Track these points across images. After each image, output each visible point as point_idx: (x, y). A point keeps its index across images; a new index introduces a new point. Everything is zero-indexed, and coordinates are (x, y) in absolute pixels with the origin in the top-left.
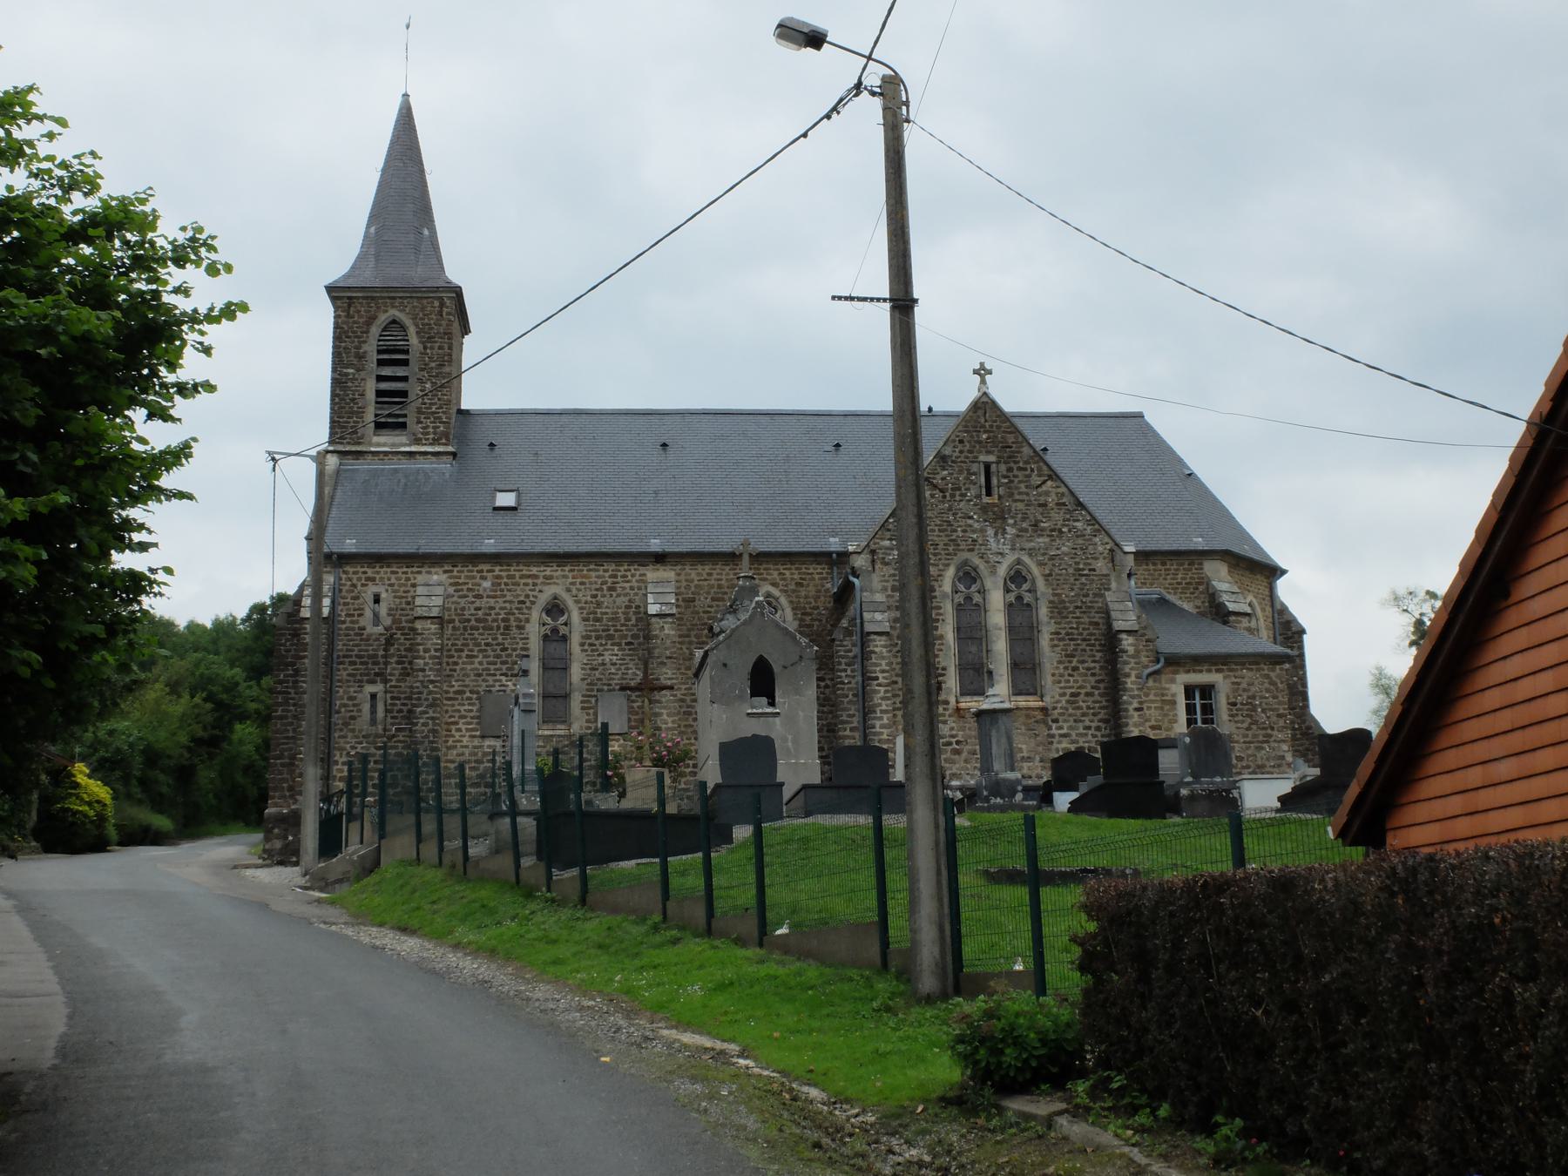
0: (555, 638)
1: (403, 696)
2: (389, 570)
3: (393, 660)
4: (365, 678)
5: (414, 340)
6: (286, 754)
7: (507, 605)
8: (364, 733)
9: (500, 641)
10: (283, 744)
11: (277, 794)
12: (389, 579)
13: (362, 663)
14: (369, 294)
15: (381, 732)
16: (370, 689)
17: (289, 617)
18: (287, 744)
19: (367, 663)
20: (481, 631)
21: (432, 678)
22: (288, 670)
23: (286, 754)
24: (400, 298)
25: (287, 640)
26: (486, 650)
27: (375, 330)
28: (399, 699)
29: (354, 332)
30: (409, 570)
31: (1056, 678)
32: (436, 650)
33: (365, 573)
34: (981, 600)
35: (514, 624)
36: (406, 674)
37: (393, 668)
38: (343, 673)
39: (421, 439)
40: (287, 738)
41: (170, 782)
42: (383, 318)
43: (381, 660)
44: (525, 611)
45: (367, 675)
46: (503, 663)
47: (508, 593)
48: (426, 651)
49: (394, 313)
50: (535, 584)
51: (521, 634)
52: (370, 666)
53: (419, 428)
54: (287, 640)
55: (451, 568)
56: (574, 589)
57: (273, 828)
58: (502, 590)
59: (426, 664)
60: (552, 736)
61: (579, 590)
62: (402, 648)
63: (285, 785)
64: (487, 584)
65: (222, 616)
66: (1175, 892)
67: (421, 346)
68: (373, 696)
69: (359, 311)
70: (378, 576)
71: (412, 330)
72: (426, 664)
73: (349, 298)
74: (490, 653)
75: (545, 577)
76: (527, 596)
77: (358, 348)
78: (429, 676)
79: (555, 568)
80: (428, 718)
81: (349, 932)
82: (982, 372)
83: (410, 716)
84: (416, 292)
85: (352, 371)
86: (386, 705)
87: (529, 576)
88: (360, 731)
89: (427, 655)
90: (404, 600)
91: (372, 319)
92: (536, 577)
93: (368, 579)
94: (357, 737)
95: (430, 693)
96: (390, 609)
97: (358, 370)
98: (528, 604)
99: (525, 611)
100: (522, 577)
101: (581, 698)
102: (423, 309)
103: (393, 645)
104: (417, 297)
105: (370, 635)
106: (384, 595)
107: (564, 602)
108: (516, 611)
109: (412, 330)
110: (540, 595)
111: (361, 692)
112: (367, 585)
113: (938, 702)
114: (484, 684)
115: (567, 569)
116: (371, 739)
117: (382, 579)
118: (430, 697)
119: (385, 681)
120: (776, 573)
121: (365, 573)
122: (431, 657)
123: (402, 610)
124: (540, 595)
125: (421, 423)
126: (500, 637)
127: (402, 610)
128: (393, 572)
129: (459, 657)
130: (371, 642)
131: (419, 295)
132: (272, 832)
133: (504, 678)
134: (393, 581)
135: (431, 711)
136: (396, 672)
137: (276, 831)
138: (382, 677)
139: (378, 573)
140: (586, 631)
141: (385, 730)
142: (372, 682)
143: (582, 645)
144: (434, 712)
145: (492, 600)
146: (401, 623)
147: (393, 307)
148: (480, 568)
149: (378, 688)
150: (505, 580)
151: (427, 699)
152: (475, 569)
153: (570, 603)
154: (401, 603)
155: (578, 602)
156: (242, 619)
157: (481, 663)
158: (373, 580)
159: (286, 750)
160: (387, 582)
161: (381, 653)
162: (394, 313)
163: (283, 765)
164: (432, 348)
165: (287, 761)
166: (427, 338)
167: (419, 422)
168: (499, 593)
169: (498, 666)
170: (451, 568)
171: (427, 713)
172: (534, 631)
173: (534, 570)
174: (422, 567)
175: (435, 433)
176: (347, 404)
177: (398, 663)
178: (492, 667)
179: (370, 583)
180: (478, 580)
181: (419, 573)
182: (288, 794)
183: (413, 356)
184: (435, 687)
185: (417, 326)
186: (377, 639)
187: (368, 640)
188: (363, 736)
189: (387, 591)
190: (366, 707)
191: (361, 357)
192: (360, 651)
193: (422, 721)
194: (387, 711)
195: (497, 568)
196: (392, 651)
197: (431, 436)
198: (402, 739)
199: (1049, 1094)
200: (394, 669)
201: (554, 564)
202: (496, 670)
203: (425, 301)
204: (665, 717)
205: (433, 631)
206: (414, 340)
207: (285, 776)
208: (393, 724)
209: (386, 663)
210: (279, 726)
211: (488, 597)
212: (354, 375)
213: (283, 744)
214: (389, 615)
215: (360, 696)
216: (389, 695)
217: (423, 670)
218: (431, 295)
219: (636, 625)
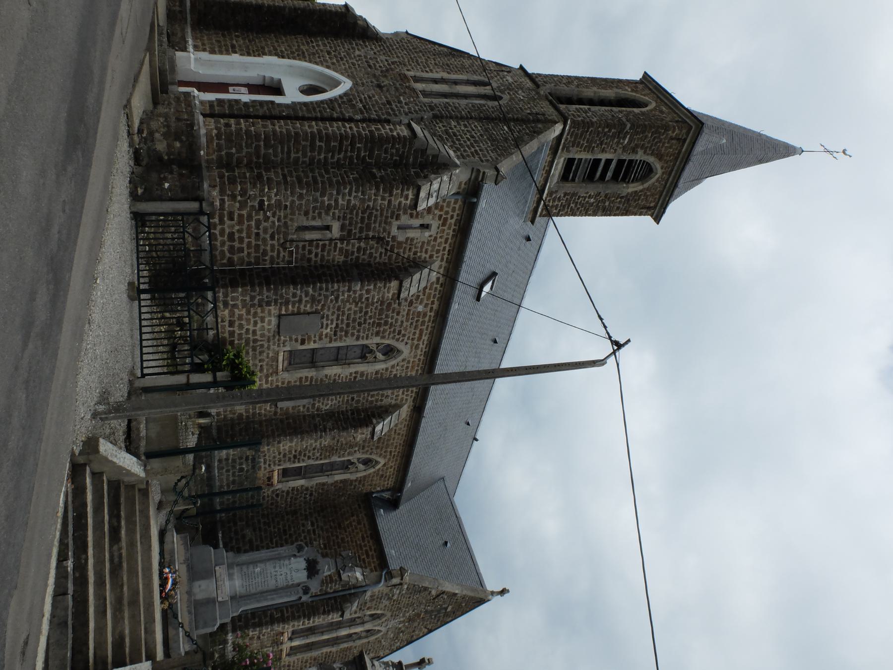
0: (365, 354)
1: (325, 254)
2: (450, 237)
3: (362, 244)
4: (347, 222)
6: (271, 151)
7: (399, 323)
8: (289, 223)
9: (368, 321)
10: (282, 148)
11: (223, 142)
12: (441, 237)
13: (363, 218)
14: (681, 156)
15: (290, 237)
16: (336, 226)
17: (422, 150)
18: (282, 152)
19: (362, 222)
20: (379, 307)
21: (341, 298)
22: (365, 152)
23: (271, 151)
24: (668, 179)
25: (397, 150)
26: (361, 312)
28: (323, 250)
29: (656, 143)
30: (446, 252)
31: (296, 461)
32: (367, 299)
33: (452, 217)
34: (358, 623)
35: (382, 329)
39: (551, 196)
40: (289, 152)
43: (363, 235)
44: (392, 335)
45: (350, 224)
46: (348, 325)
47: (409, 324)
48: (368, 292)
50: (413, 339)
51: (372, 334)
52: (359, 225)
53: (561, 194)
54: (397, 150)
55: (440, 282)
56: (405, 363)
57: (181, 141)
58: (412, 319)
59: (355, 292)
60: (277, 362)
61: (402, 366)
62: (374, 251)
63: (234, 151)
64: (420, 308)
67: (624, 194)
68: (328, 228)
69: (670, 147)
70: (445, 228)
72: (355, 292)
73: (685, 140)
74: (358, 315)
75: (417, 346)
76: (404, 335)
77: (642, 147)
78: (343, 295)
79: (424, 350)
80: (301, 296)
82: (503, 592)
84: (668, 192)
85: (626, 142)
86: (317, 240)
87: (421, 335)
88: (292, 220)
89: (364, 292)
90: (419, 250)
92: (419, 339)
93: (446, 220)
94: (285, 217)
95: (326, 297)
96: (412, 239)
97: (624, 148)
98: (397, 337)
99: (392, 335)
100: (421, 331)
101: (310, 376)
102: (652, 195)
103: (377, 243)
104: (663, 193)
105: (390, 224)
106: (427, 234)
107: (395, 358)
108: (392, 330)
110: (404, 343)
111: (334, 218)
112: (440, 219)
113: (290, 559)
114: (330, 313)
115: (422, 357)
116: (283, 230)
117: (443, 231)
118: (322, 297)
119: (342, 239)
120: (393, 464)
121: (452, 217)
122: (361, 296)
123: (410, 249)
124: (404, 343)
125: (564, 196)
126: (371, 321)
127: (410, 249)
128: (447, 240)
129: (365, 546)
130: (383, 225)
131: (664, 193)
132: (176, 140)
133: (334, 326)
134: (439, 240)
135: (308, 299)
136: (350, 247)
137: (178, 144)
139: (449, 228)
140: (367, 374)
141: (292, 241)
142: (342, 228)
143: (356, 373)
144: (306, 301)
145: (405, 313)
146: (397, 248)
147: (663, 173)
148: (436, 302)
149: (336, 232)
150: (412, 253)
151: (320, 295)
152: (436, 300)
153: (393, 362)
154: (416, 247)
155: (393, 367)
157: (350, 309)
158: (444, 224)
159: (275, 151)
160: (439, 235)
161: (371, 234)
163: (258, 147)
164: (620, 202)
165: (263, 151)
167: (565, 194)
168: (411, 317)
169: (345, 321)
170: (440, 282)
171: (306, 296)
172: (373, 341)
173: (425, 338)
174: (446, 262)
175: (552, 206)
176: (600, 138)
177: (359, 249)
178: (345, 318)
179: (441, 222)
180: (425, 301)
181: (442, 260)
182: (223, 153)
184: (332, 301)
185: (641, 191)
186: (384, 230)
187: (386, 223)
188: (286, 223)
189: (430, 236)
190: (318, 223)
192: (376, 216)
193: (299, 292)
194: (311, 242)
195: (432, 314)
196: (371, 242)
197: (551, 204)
198: (281, 255)
200: (353, 245)
201: (427, 350)
202: (342, 320)
203: (657, 197)
204: (289, 444)
205: (387, 295)
207: (245, 150)
208: (297, 247)
209: (360, 239)
210: (303, 143)
211: (409, 310)
212: (622, 144)
213: (282, 148)
214: (407, 239)
215: (329, 218)
216: (327, 242)
217: (349, 290)
218: (660, 202)
219: (367, 401)
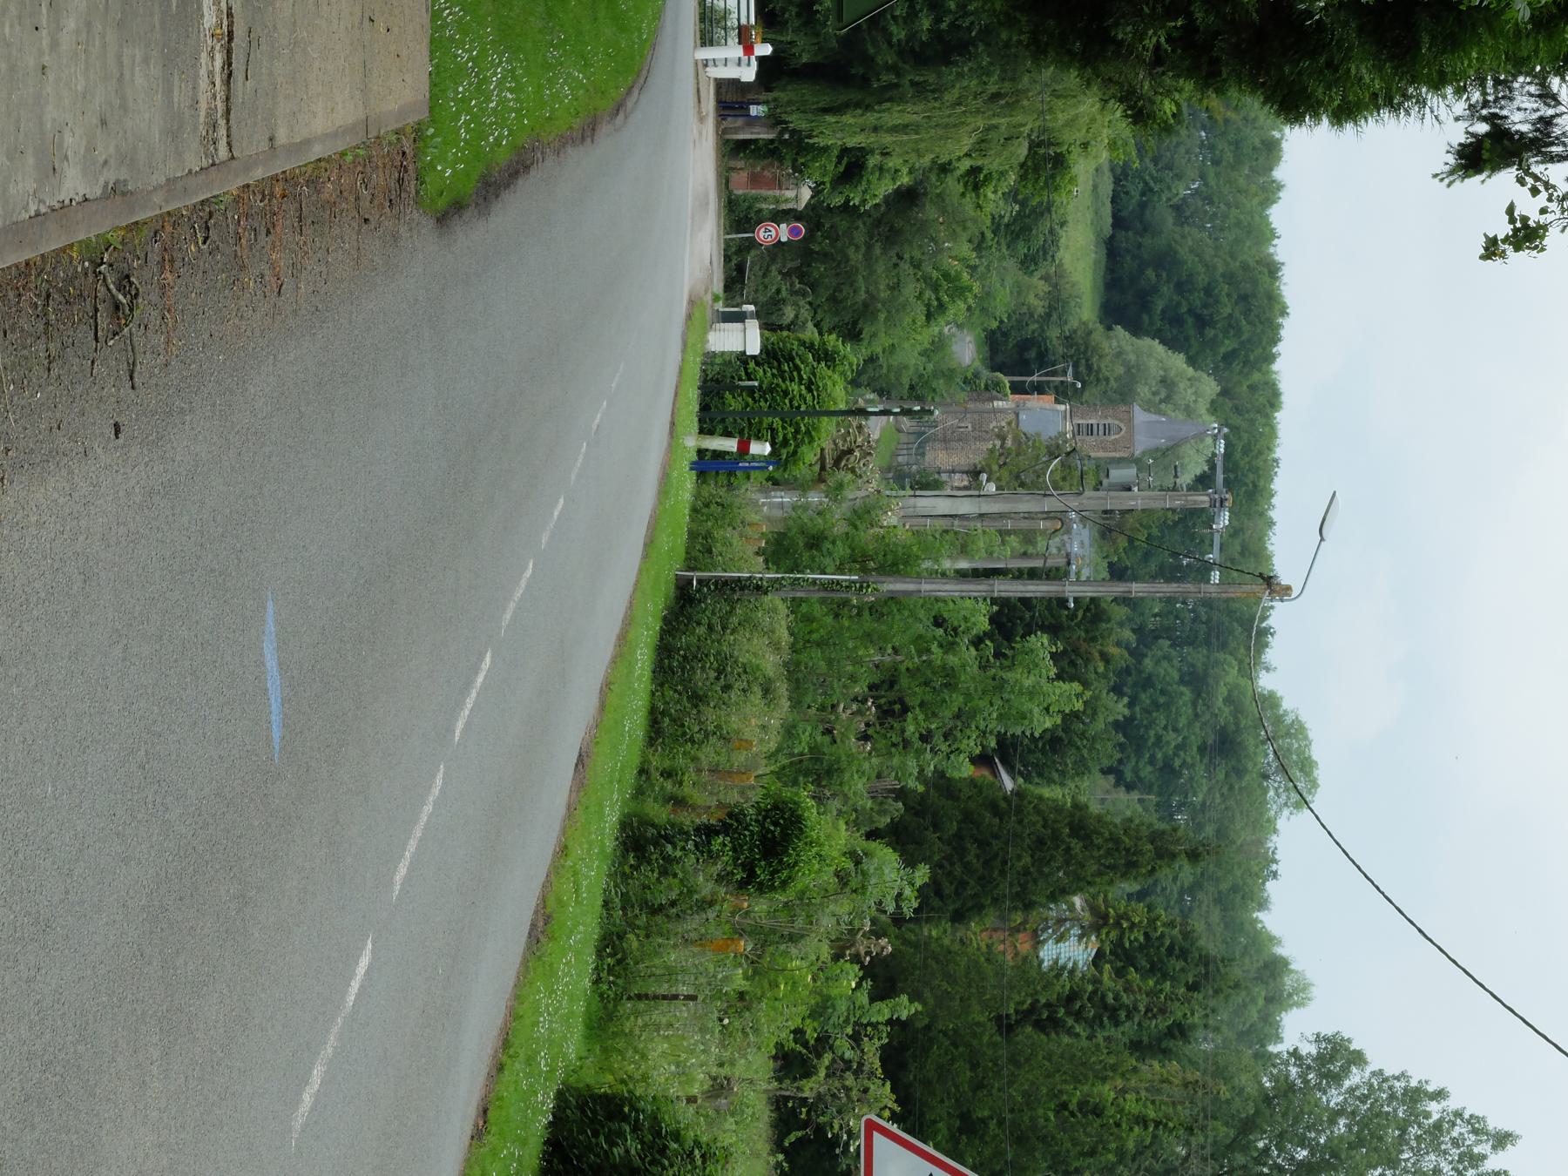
5: (1113, 437)
27: (1117, 422)
36: (975, 438)
37: (977, 433)
38: (976, 416)
41: (1169, 688)
42: (1122, 425)
49: (1124, 428)
65: (1274, 501)
66: (951, 296)
71: (1117, 437)
81: (878, 428)
83: (960, 440)
91: (1121, 421)
109: (1117, 437)
138: (974, 429)
149: (970, 428)
156: (1188, 485)
162: (1124, 428)
166: (1114, 443)
183: (1107, 438)
191: (1106, 417)
199: (494, 1057)
206: (1113, 437)
